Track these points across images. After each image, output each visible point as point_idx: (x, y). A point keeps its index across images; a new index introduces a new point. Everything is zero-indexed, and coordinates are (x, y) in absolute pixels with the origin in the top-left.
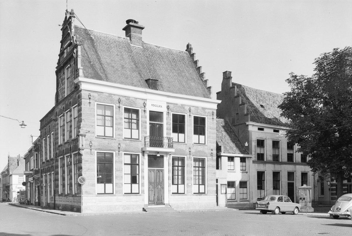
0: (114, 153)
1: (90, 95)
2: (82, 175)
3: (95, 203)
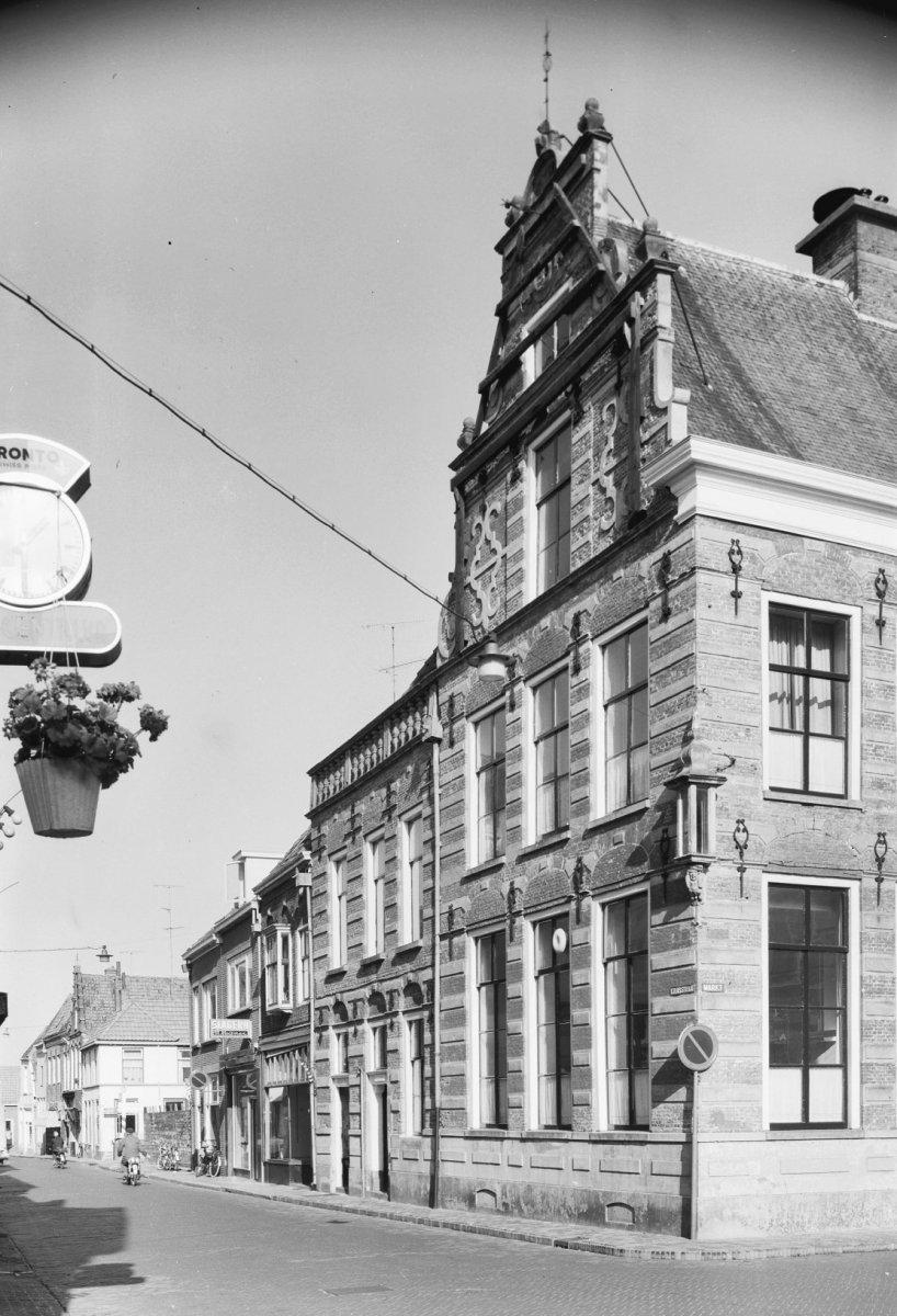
0: (854, 888)
1: (735, 550)
2: (694, 1019)
3: (762, 1180)
